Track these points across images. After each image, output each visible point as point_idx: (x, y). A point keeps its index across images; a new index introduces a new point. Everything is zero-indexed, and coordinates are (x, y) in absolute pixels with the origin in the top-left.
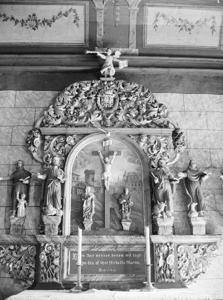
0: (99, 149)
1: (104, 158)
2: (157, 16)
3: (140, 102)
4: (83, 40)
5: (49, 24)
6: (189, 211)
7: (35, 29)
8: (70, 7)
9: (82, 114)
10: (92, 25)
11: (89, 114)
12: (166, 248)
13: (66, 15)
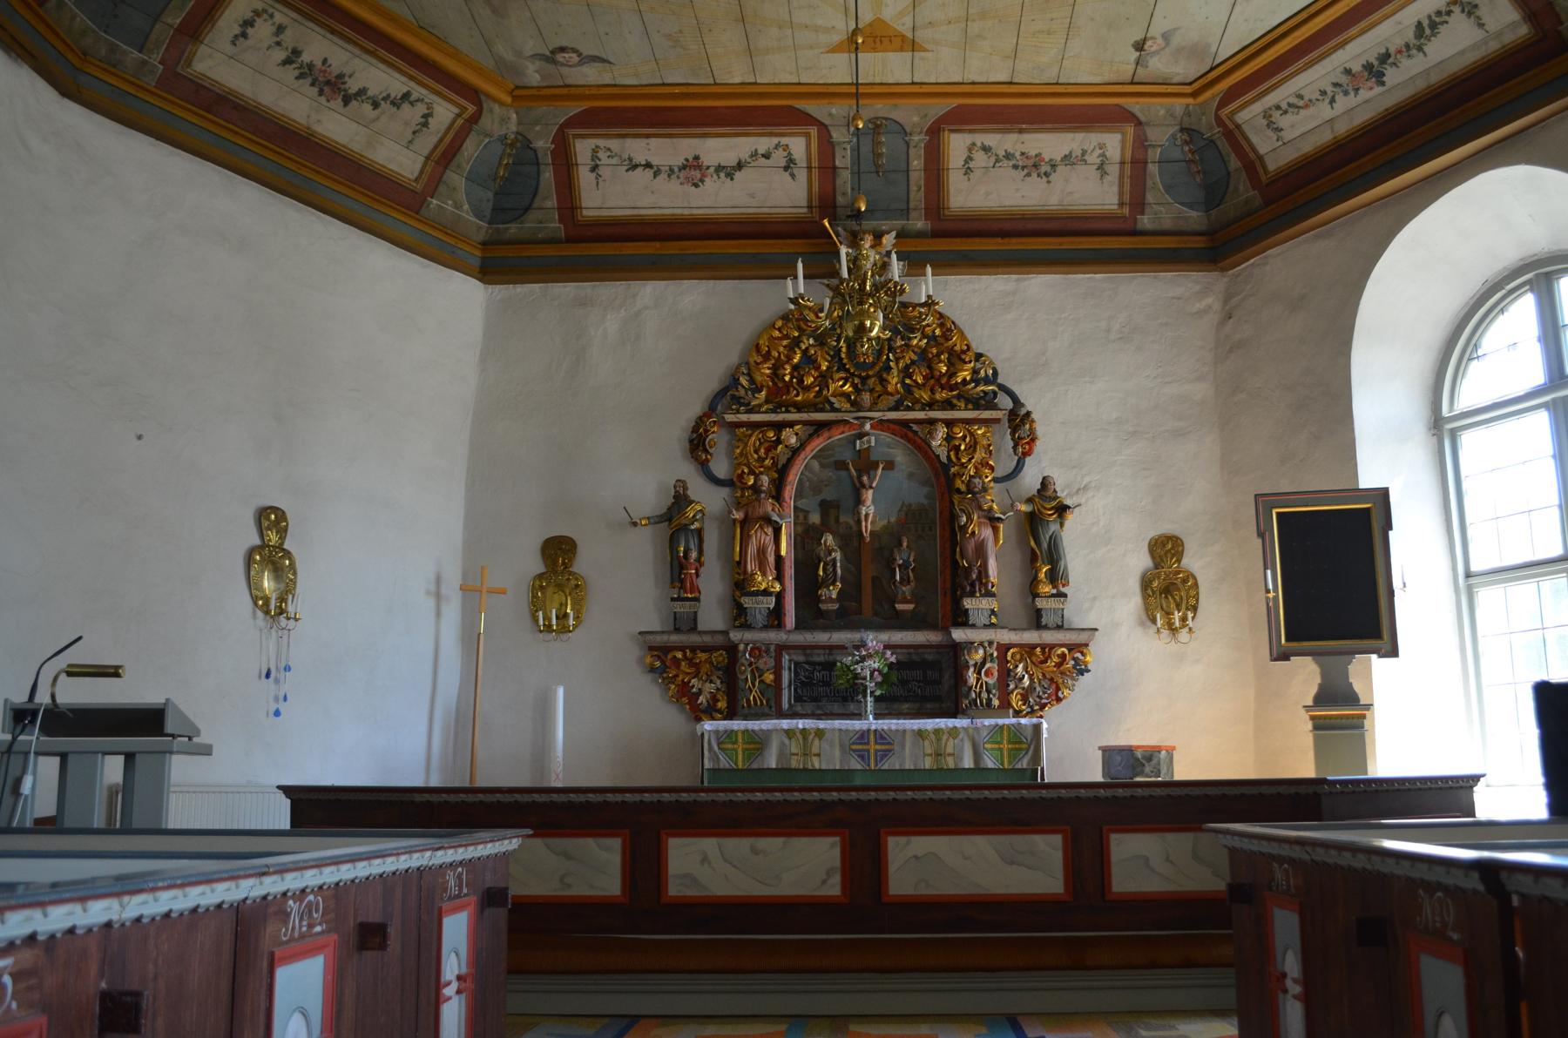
0: (847, 456)
1: (860, 477)
2: (970, 150)
3: (934, 351)
4: (805, 203)
5: (730, 176)
6: (1034, 582)
7: (696, 186)
8: (775, 140)
9: (809, 380)
10: (826, 168)
11: (824, 380)
12: (981, 652)
13: (767, 156)
